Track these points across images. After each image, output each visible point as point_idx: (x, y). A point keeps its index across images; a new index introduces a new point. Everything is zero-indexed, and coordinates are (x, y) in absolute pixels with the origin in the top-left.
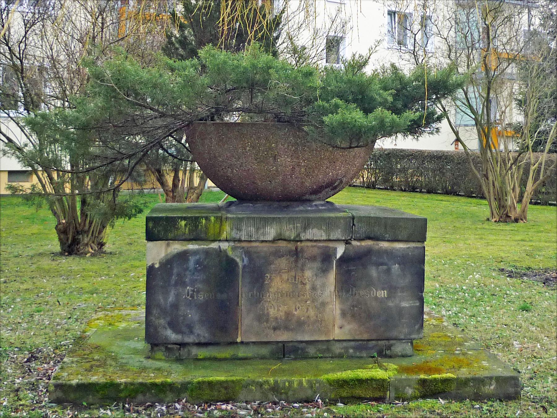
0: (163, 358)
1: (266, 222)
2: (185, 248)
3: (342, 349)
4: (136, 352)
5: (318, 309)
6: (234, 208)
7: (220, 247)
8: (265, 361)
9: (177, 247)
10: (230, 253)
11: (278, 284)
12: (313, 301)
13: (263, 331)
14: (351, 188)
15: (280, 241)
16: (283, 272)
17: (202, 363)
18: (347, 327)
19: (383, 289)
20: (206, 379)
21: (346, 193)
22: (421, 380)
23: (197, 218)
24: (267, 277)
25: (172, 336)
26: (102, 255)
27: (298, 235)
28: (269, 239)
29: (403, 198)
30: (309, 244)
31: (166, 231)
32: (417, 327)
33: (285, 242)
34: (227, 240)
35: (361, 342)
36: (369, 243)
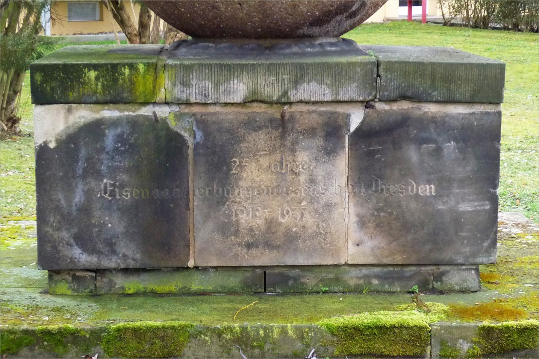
0: (69, 292)
1: (231, 71)
2: (97, 116)
3: (360, 278)
4: (29, 283)
5: (320, 214)
6: (184, 50)
7: (154, 113)
8: (232, 297)
9: (84, 115)
10: (172, 124)
11: (254, 173)
12: (311, 203)
13: (230, 249)
14: (445, 27)
15: (255, 104)
16: (260, 155)
17: (130, 300)
18: (369, 244)
19: (429, 182)
20: (131, 325)
21: (436, 37)
22: (484, 328)
23: (115, 66)
24: (235, 162)
25: (83, 258)
26: (14, 137)
27: (285, 93)
28: (235, 101)
29: (532, 44)
30: (304, 108)
31: (65, 90)
32: (486, 244)
33: (263, 106)
34: (166, 103)
35: (391, 269)
36: (405, 105)
